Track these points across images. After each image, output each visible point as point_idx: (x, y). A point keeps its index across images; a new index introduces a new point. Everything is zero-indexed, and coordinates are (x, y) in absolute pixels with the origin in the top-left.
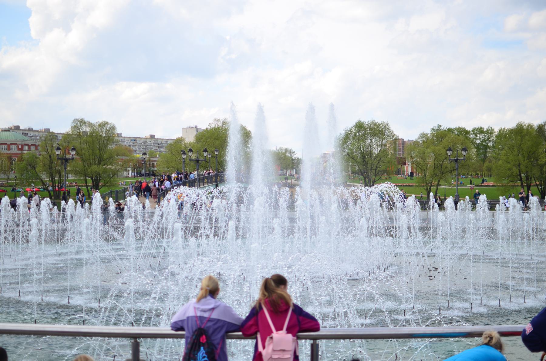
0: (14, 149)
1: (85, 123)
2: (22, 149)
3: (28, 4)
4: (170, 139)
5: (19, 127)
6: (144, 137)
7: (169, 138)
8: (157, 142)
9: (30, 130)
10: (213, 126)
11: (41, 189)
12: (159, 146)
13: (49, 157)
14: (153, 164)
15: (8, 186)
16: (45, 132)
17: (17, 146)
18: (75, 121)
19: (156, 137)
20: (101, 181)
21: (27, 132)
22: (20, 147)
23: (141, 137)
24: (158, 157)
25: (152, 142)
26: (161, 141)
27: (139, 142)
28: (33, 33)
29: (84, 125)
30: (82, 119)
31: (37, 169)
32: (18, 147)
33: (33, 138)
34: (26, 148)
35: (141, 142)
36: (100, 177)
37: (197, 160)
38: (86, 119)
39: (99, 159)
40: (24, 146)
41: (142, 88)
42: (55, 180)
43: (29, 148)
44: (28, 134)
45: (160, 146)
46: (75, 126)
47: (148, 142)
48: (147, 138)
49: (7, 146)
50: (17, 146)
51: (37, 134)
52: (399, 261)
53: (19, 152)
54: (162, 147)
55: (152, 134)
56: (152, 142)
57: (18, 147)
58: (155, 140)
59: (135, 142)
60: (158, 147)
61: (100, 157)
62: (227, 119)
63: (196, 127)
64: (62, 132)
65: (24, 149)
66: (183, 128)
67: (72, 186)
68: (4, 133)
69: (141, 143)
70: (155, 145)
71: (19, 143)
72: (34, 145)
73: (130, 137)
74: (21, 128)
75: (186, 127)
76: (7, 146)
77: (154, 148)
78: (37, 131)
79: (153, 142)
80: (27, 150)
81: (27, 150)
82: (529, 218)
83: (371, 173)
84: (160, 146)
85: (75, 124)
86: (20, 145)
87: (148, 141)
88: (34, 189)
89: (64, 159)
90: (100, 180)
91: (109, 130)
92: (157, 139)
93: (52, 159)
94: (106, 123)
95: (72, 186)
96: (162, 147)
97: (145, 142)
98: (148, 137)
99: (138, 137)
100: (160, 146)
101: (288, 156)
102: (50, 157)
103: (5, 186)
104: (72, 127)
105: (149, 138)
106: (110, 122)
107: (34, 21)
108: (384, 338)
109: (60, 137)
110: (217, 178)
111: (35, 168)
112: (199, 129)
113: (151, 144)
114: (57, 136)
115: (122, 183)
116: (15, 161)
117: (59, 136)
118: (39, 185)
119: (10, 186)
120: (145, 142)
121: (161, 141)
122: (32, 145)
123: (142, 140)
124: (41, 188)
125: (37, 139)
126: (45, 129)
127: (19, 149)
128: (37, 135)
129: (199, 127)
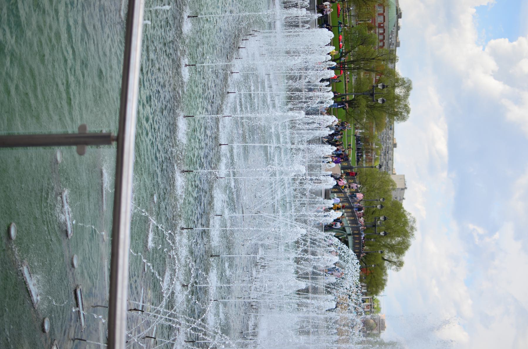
0: (380, 19)
1: (408, 91)
2: (379, 27)
3: (521, 39)
5: (400, 17)
6: (394, 137)
8: (390, 149)
9: (398, 28)
10: (408, 217)
11: (341, 50)
13: (373, 57)
14: (369, 152)
15: (343, 17)
16: (396, 42)
17: (383, 22)
18: (410, 82)
19: (394, 149)
20: (351, 108)
22: (382, 25)
23: (395, 134)
24: (376, 156)
25: (390, 145)
26: (391, 154)
27: (389, 133)
28: (493, 42)
29: (406, 90)
30: (411, 88)
31: (361, 46)
32: (382, 24)
34: (381, 31)
35: (389, 134)
36: (355, 107)
37: (376, 225)
38: (411, 92)
39: (373, 106)
40: (382, 29)
41: (442, 146)
42: (351, 64)
43: (381, 34)
46: (405, 81)
47: (390, 141)
48: (393, 140)
49: (382, 12)
50: (383, 22)
51: (394, 35)
52: (193, 115)
53: (377, 25)
55: (398, 145)
56: (390, 145)
57: (382, 24)
61: (375, 107)
62: (416, 230)
63: (406, 188)
64: (396, 67)
65: (379, 29)
66: (404, 175)
67: (345, 78)
69: (388, 135)
70: (387, 149)
71: (386, 24)
72: (384, 45)
74: (399, 19)
75: (405, 178)
76: (382, 12)
77: (384, 148)
78: (397, 35)
79: (390, 146)
80: (379, 32)
81: (379, 32)
85: (406, 82)
87: (391, 141)
88: (341, 43)
89: (373, 92)
90: (352, 107)
91: (401, 114)
92: (393, 150)
93: (372, 60)
94: (408, 112)
95: (345, 78)
97: (389, 138)
98: (394, 141)
99: (394, 132)
100: (386, 153)
102: (374, 59)
103: (343, 15)
104: (403, 78)
105: (393, 142)
106: (409, 115)
107: (503, 43)
108: (116, 188)
110: (357, 235)
111: (362, 44)
113: (388, 144)
115: (350, 127)
116: (368, 21)
118: (345, 48)
119: (344, 19)
120: (389, 138)
122: (384, 37)
123: (391, 136)
124: (342, 50)
126: (399, 42)
127: (379, 24)
128: (393, 35)
129: (406, 191)
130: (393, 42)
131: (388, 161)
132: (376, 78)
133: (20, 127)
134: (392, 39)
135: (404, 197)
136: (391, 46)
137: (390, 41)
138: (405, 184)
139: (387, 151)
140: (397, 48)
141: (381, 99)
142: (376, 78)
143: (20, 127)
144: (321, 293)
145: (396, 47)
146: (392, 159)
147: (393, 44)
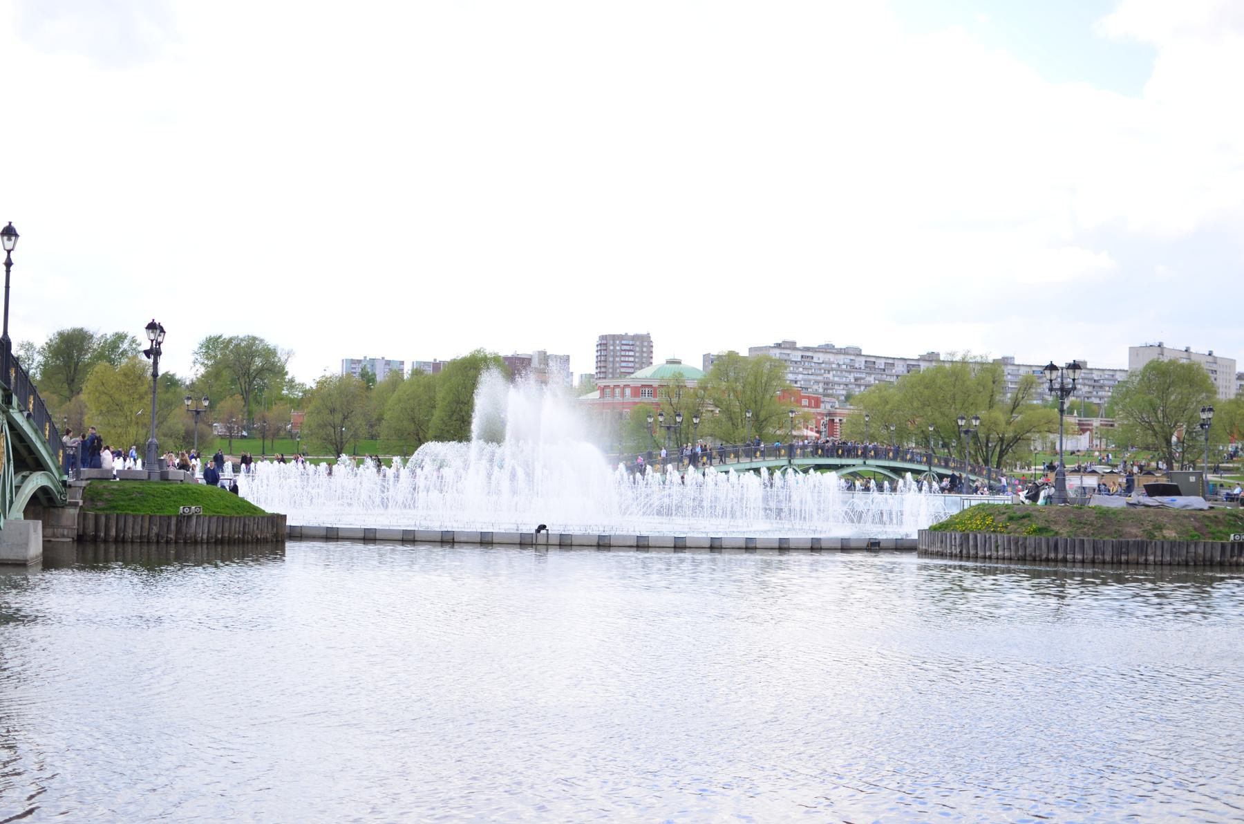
4: (1120, 370)
7: (1118, 368)
8: (1090, 376)
12: (1095, 384)
19: (1089, 366)
21: (810, 354)
33: (823, 365)
44: (812, 358)
45: (1098, 384)
54: (1101, 387)
58: (1086, 371)
59: (1042, 377)
60: (1094, 387)
68: (668, 365)
70: (1086, 382)
73: (1030, 366)
75: (1138, 345)
82: (193, 535)
83: (41, 496)
84: (1098, 384)
86: (691, 388)
96: (1101, 387)
101: (126, 476)
109: (881, 364)
112: (1165, 350)
114: (874, 362)
117: (878, 361)
121: (1099, 373)
125: (832, 369)
130: (847, 361)
131: (1115, 380)
132: (805, 406)
133: (884, 815)
134: (841, 363)
135: (1184, 349)
136: (857, 365)
137: (844, 367)
138: (1151, 346)
139: (1092, 383)
140: (798, 345)
141: (186, 401)
142: (805, 406)
143: (884, 815)
144: (174, 516)
145: (860, 355)
146: (1111, 373)
147: (851, 360)
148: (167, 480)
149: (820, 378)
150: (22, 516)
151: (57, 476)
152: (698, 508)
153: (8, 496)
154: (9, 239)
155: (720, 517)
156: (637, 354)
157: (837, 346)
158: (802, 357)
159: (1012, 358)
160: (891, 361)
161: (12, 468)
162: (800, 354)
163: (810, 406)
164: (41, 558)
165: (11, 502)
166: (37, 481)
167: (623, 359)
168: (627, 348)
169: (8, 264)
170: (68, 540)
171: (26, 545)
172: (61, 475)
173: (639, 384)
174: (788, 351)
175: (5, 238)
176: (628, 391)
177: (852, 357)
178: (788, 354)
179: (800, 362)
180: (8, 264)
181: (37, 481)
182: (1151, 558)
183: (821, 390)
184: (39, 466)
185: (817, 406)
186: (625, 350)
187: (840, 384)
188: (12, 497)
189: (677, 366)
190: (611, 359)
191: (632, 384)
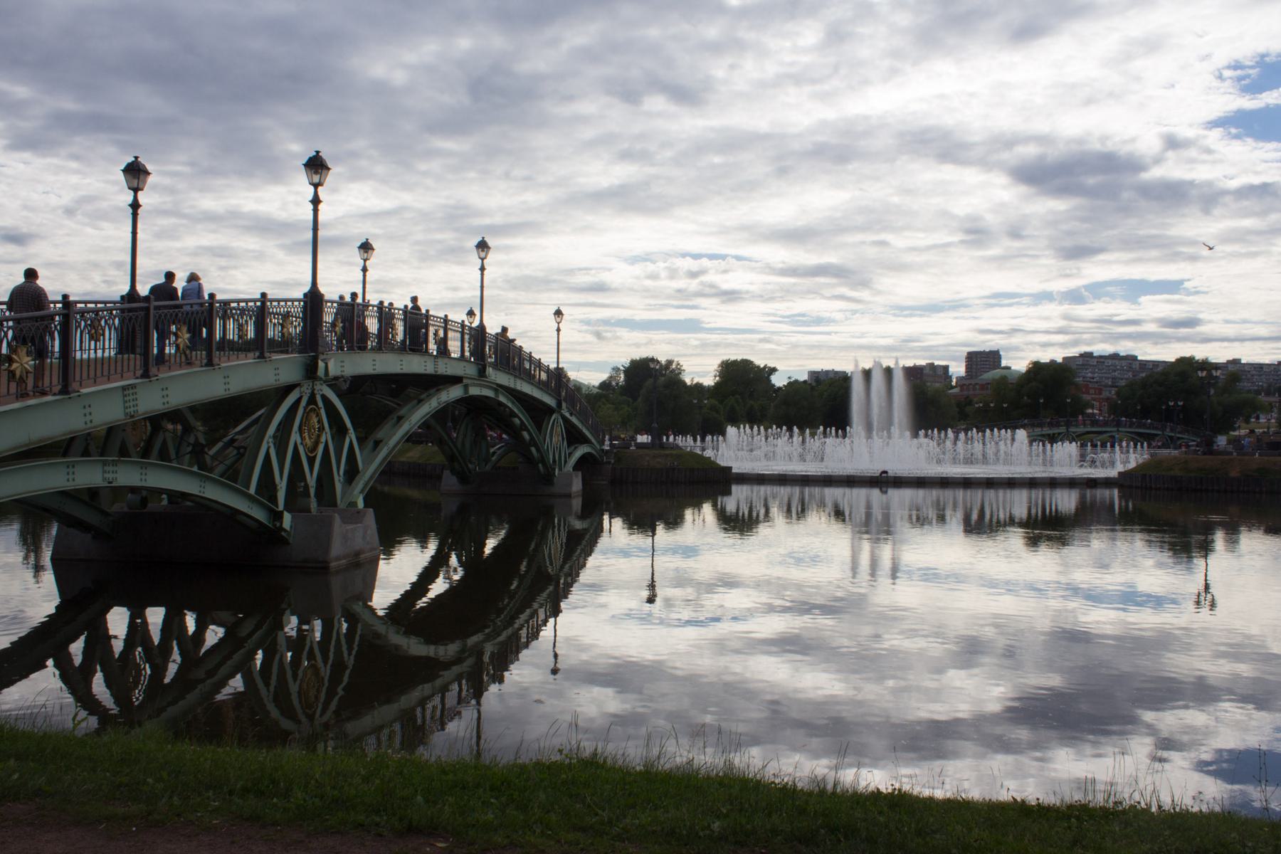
21: (1102, 360)
44: (1104, 362)
125: (1118, 370)
142: (1092, 394)
148: (663, 448)
149: (1109, 375)
150: (571, 470)
151: (598, 447)
152: (985, 459)
153: (563, 458)
154: (559, 317)
155: (772, 459)
156: (991, 363)
157: (1122, 354)
158: (1097, 362)
159: (1240, 360)
160: (1156, 363)
161: (565, 443)
162: (1096, 360)
163: (1095, 394)
164: (580, 493)
165: (566, 462)
166: (581, 450)
167: (982, 366)
168: (985, 359)
169: (558, 330)
170: (605, 482)
171: (570, 485)
172: (601, 446)
173: (984, 382)
174: (1088, 359)
175: (480, 250)
176: (977, 387)
177: (1130, 362)
178: (1088, 361)
179: (1096, 366)
180: (558, 330)
181: (581, 450)
182: (1264, 489)
183: (1110, 383)
184: (585, 441)
185: (1100, 394)
186: (984, 361)
187: (1122, 379)
188: (565, 458)
189: (1008, 370)
190: (974, 366)
191: (980, 382)
